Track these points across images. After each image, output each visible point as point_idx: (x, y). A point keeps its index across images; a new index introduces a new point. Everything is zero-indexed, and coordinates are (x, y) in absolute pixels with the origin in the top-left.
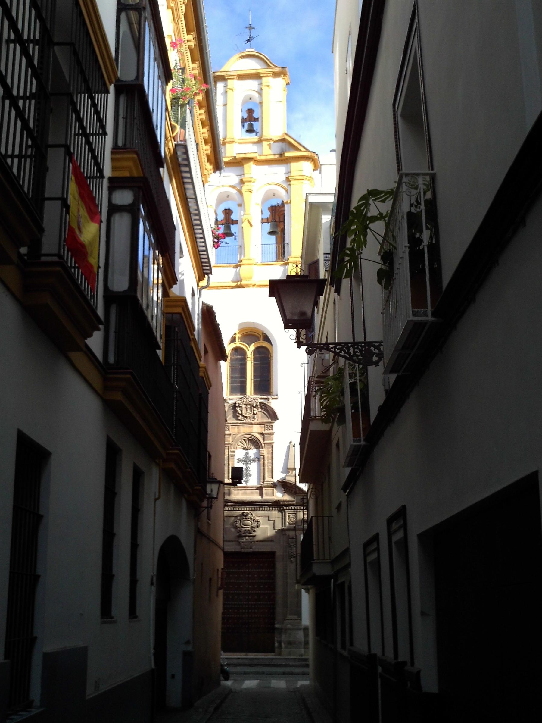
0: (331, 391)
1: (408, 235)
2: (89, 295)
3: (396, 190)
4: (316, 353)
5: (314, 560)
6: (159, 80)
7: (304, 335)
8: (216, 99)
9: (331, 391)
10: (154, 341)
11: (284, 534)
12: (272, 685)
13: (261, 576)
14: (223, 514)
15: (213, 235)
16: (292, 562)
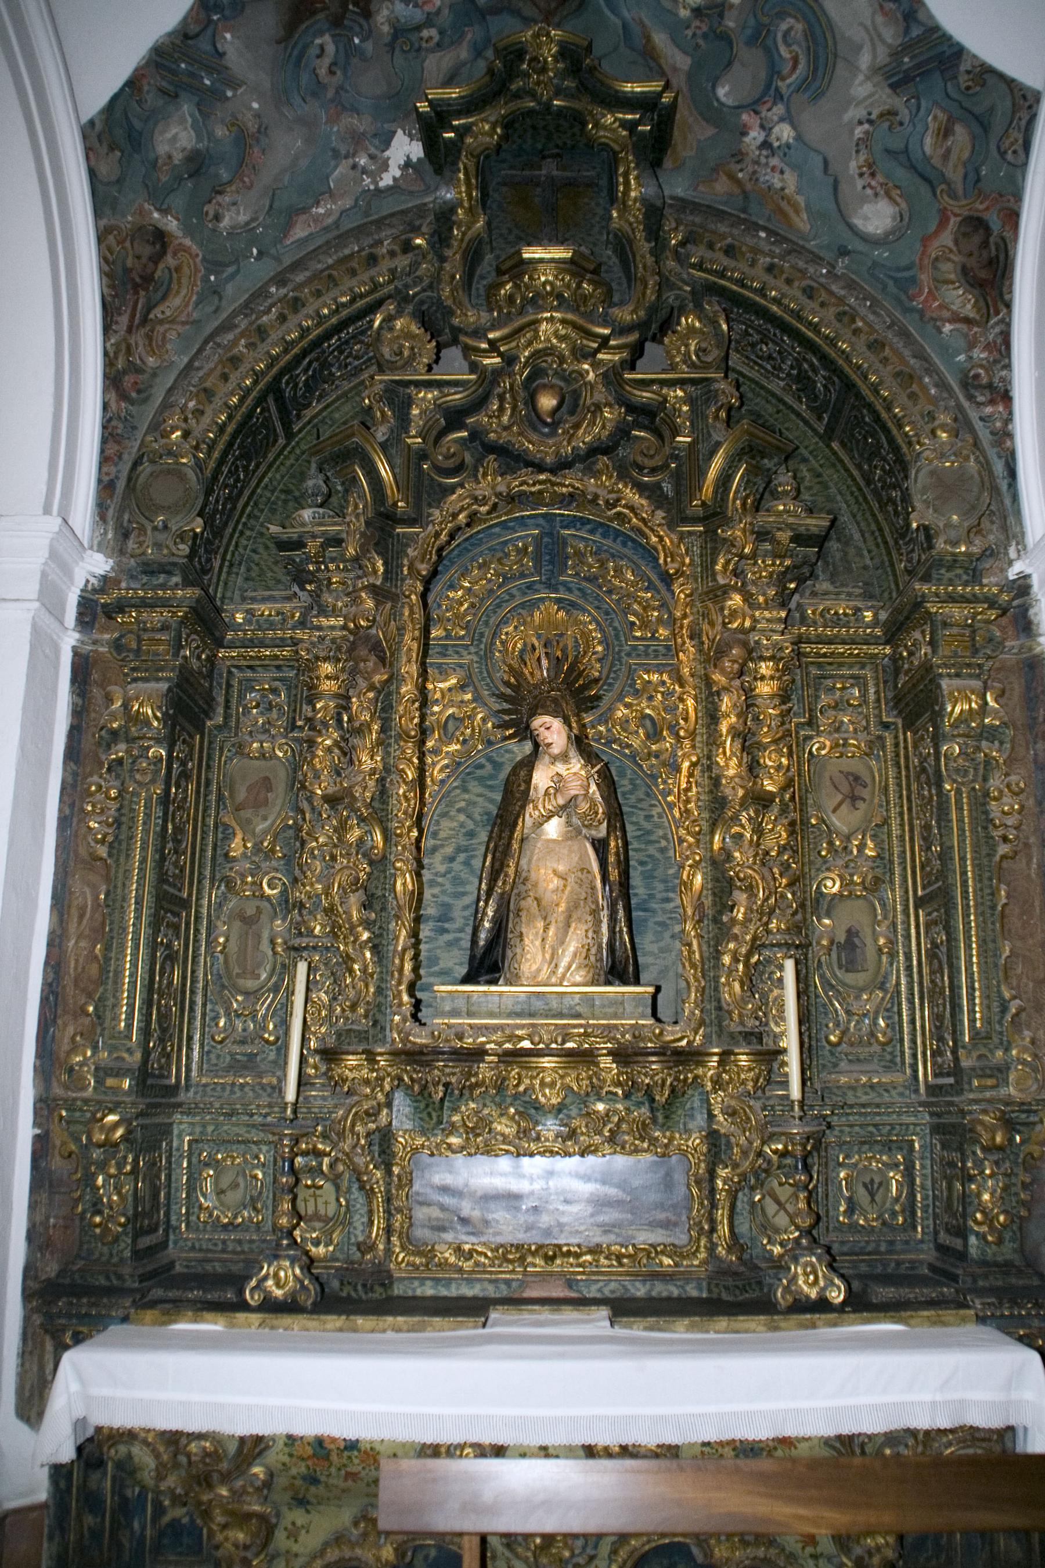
0: (255, 251)
1: (73, 664)
2: (108, 1515)
3: (180, 1274)
4: (612, 1266)
5: (578, 715)
6: (618, 1186)
7: (42, 1466)
8: (291, 1439)
9: (255, 251)
10: (499, 131)
11: (903, 156)
12: (422, 155)
13: (123, 1220)
14: (351, 1048)
15: (533, 1248)
16: (315, 858)
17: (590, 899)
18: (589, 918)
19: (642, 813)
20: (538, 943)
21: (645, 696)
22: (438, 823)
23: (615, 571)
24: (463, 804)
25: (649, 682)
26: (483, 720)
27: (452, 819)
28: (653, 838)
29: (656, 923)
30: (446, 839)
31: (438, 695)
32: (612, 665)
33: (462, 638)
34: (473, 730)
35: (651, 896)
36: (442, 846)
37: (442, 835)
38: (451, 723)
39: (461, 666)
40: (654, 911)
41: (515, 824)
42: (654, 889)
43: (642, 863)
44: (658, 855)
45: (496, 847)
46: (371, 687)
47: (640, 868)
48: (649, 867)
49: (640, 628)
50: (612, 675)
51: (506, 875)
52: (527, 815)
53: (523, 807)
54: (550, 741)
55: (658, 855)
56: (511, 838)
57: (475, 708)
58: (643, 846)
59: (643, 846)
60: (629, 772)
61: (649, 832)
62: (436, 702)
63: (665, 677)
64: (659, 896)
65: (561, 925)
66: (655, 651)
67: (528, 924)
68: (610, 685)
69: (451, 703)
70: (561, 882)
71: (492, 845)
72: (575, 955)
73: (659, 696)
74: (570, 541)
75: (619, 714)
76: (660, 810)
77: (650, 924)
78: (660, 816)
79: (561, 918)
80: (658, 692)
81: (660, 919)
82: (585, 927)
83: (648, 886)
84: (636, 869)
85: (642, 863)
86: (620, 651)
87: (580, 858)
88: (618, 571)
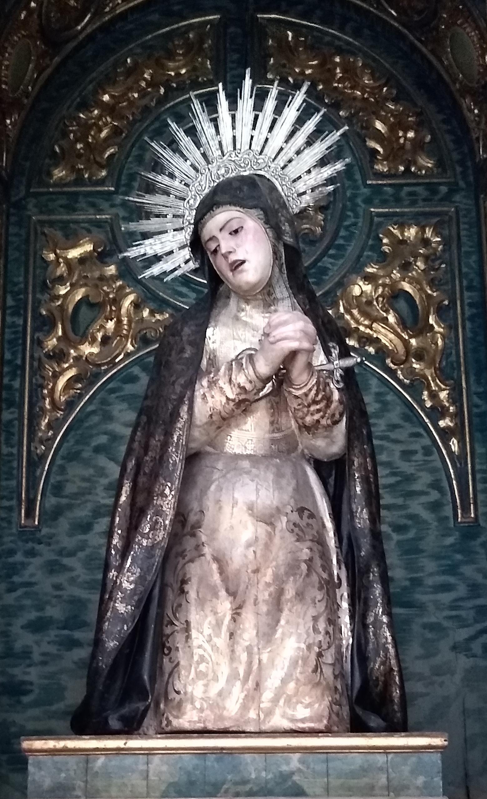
17: (318, 562)
18: (319, 595)
19: (398, 448)
20: (222, 641)
21: (397, 262)
22: (62, 470)
23: (344, 71)
24: (103, 439)
25: (403, 242)
26: (137, 306)
27: (87, 463)
28: (417, 487)
29: (425, 626)
30: (75, 496)
31: (62, 269)
32: (343, 217)
33: (102, 182)
34: (119, 322)
35: (416, 582)
36: (70, 507)
37: (70, 489)
38: (84, 309)
39: (99, 224)
40: (421, 607)
41: (175, 415)
42: (421, 569)
43: (399, 529)
44: (425, 515)
45: (139, 466)
46: (142, 540)
47: (395, 537)
48: (411, 534)
49: (386, 158)
50: (343, 233)
51: (159, 512)
52: (198, 401)
53: (191, 385)
54: (238, 256)
55: (425, 515)
56: (165, 445)
57: (121, 288)
58: (400, 501)
59: (400, 501)
60: (374, 382)
61: (409, 479)
62: (61, 280)
63: (429, 233)
64: (430, 581)
65: (264, 608)
66: (410, 194)
67: (201, 602)
68: (340, 248)
69: (84, 281)
70: (262, 529)
71: (131, 464)
72: (294, 663)
73: (420, 264)
74: (271, 29)
75: (356, 291)
76: (427, 441)
77: (416, 628)
78: (427, 451)
79: (264, 595)
80: (416, 256)
81: (433, 619)
82: (312, 612)
83: (410, 566)
84: (389, 538)
85: (399, 529)
86: (355, 196)
87: (297, 490)
88: (347, 69)
